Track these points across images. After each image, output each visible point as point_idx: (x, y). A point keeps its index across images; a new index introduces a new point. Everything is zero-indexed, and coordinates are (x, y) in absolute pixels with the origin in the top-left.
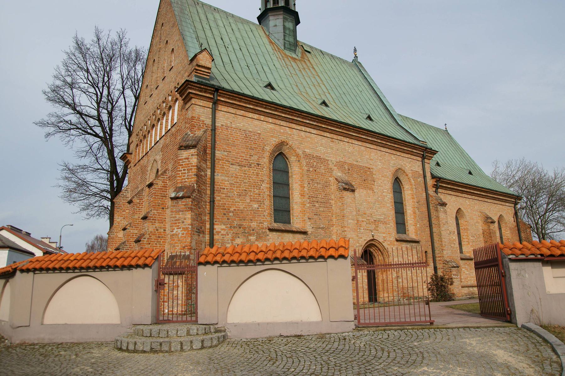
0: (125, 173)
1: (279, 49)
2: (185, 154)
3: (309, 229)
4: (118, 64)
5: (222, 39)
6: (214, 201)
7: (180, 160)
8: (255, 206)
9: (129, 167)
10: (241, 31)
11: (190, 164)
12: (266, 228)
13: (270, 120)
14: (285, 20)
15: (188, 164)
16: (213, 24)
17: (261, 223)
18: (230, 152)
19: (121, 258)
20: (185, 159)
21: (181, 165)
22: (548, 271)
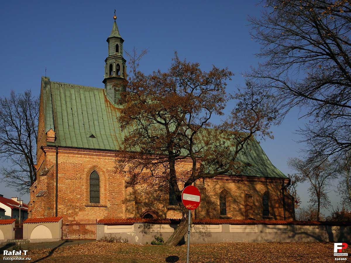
1: (110, 104)
5: (72, 109)
7: (41, 180)
8: (79, 196)
13: (88, 156)
16: (68, 100)
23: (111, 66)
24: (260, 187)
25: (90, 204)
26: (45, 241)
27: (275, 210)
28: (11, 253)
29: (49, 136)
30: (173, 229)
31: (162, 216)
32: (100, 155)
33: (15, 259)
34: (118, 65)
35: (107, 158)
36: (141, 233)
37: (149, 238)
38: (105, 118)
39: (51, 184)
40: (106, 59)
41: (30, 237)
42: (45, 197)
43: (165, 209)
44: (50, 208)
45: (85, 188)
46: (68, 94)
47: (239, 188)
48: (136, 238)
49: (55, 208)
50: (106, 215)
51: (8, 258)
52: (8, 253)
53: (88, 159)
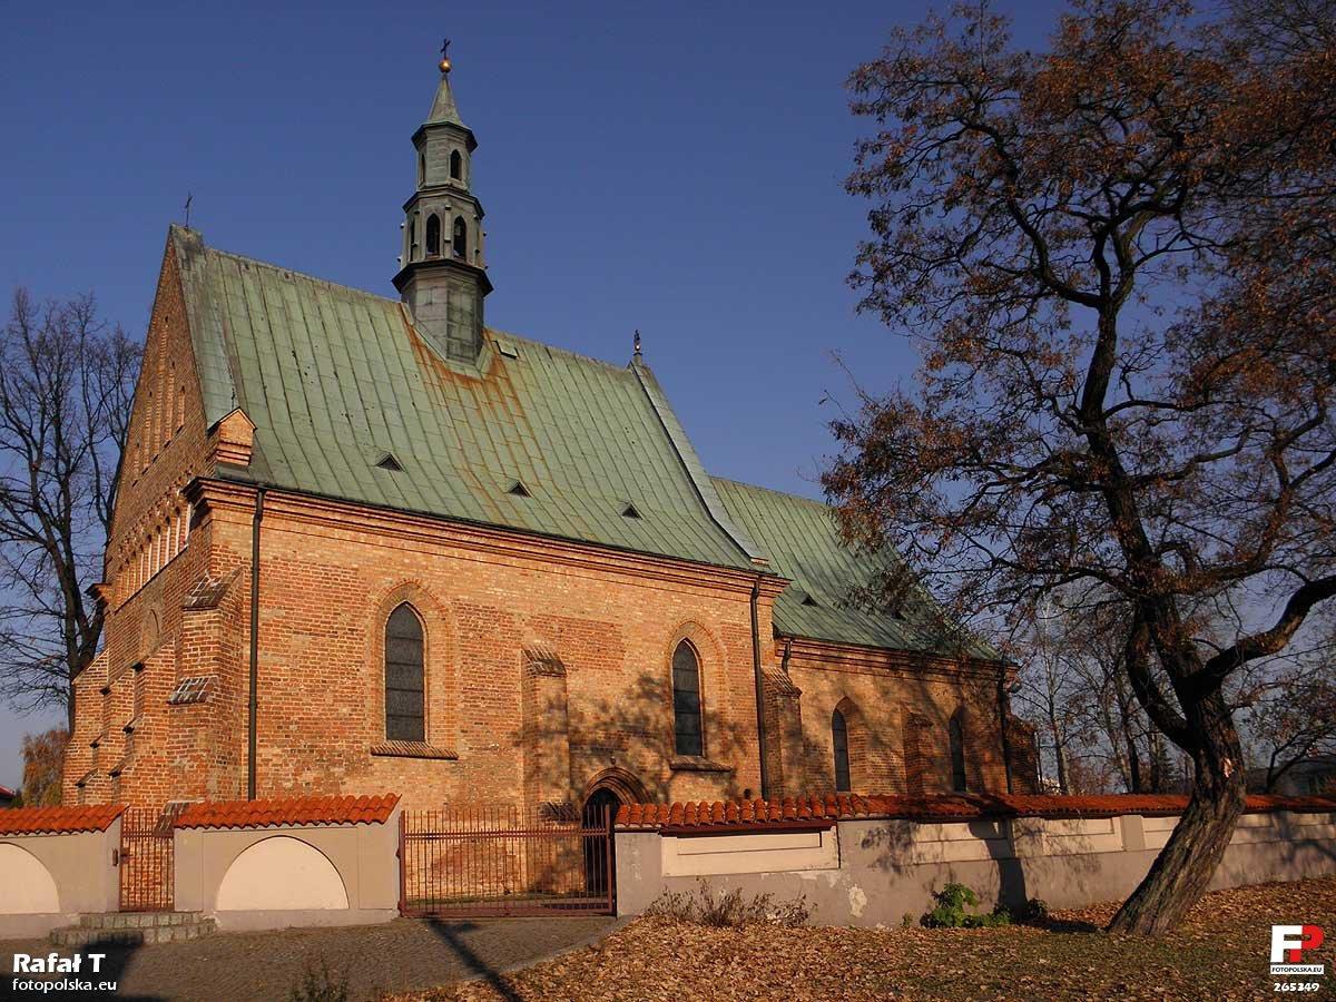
0: (100, 621)
1: (432, 359)
2: (196, 620)
3: (463, 752)
4: (77, 374)
5: (295, 356)
6: (256, 704)
7: (187, 630)
8: (345, 710)
9: (105, 612)
10: (346, 324)
11: (206, 638)
12: (367, 751)
13: (381, 540)
14: (452, 289)
15: (202, 639)
16: (277, 319)
17: (357, 742)
18: (293, 609)
19: (60, 817)
20: (196, 628)
21: (189, 640)
22: (670, 845)
23: (434, 223)
24: (941, 692)
25: (389, 744)
26: (307, 924)
27: (984, 770)
28: (41, 962)
29: (229, 437)
30: (983, 842)
31: (656, 795)
32: (431, 540)
33: (59, 986)
34: (460, 222)
35: (456, 552)
36: (879, 870)
37: (915, 899)
38: (423, 404)
39: (233, 648)
40: (412, 198)
41: (213, 899)
42: (212, 705)
43: (666, 768)
44: (228, 760)
45: (370, 675)
46: (273, 298)
47: (887, 693)
48: (852, 895)
49: (244, 759)
50: (453, 793)
51: (31, 982)
52: (29, 965)
53: (382, 553)
